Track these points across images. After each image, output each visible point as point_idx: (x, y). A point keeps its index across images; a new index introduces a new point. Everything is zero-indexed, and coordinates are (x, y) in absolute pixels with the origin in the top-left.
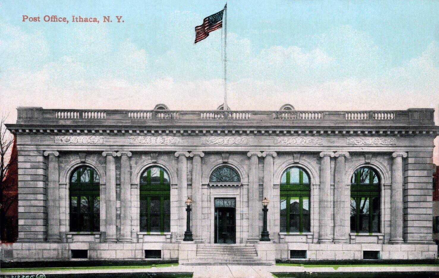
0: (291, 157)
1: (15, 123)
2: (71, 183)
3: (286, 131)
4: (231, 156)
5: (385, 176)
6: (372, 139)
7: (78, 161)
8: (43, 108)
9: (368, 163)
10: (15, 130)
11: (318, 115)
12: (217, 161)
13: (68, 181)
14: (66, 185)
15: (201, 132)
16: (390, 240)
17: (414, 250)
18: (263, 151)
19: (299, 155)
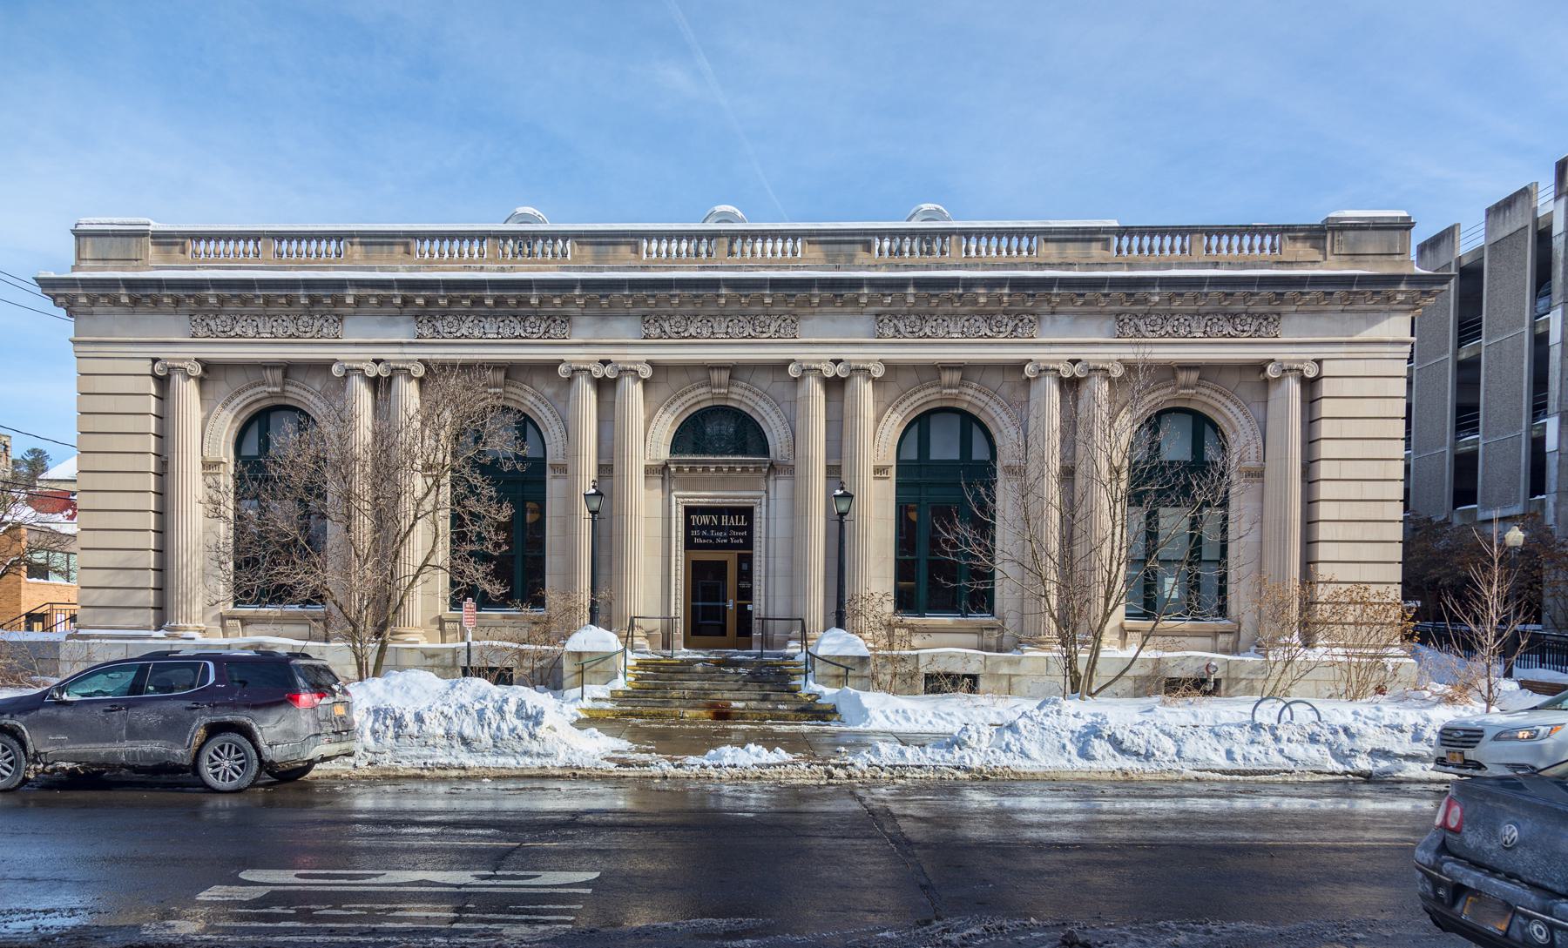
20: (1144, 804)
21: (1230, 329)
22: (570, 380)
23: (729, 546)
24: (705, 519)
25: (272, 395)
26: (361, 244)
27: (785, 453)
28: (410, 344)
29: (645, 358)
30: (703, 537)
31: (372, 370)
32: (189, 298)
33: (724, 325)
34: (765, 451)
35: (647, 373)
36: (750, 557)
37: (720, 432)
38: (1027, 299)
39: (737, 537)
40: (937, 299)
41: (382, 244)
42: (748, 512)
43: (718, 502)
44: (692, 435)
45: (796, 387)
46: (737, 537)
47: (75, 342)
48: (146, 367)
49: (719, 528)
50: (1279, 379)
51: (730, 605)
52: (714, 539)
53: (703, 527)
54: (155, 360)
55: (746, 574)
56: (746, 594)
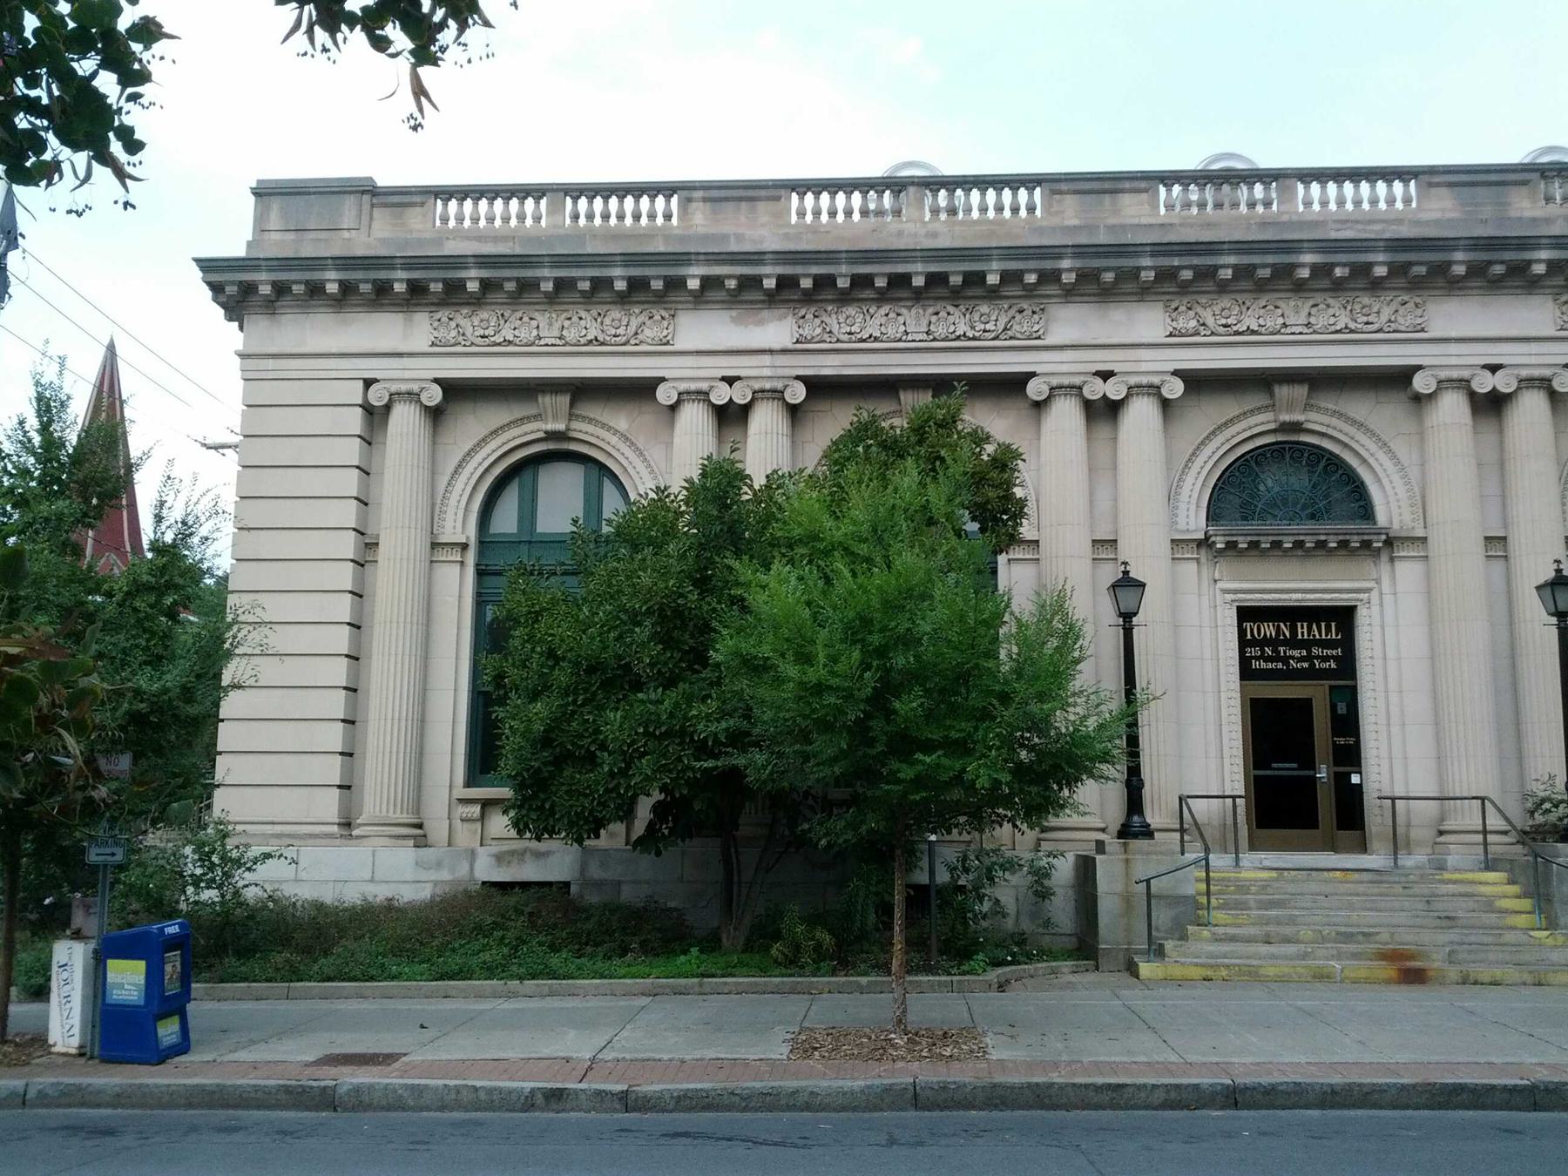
0: (1256, 400)
1: (240, 251)
2: (486, 542)
3: (623, 278)
4: (1328, 401)
5: (1390, 491)
6: (918, 319)
7: (1262, 421)
8: (379, 184)
9: (1296, 427)
10: (274, 284)
11: (1015, 195)
12: (1252, 424)
13: (472, 532)
14: (464, 547)
15: (756, 281)
16: (1441, 833)
17: (368, 876)
18: (738, 378)
19: (1301, 391)
20: (61, 1111)
21: (967, 329)
22: (673, 408)
23: (1312, 674)
24: (1268, 630)
25: (552, 436)
26: (705, 200)
27: (1407, 518)
28: (784, 351)
29: (1171, 367)
30: (1268, 659)
31: (721, 395)
32: (431, 286)
33: (557, 325)
34: (1366, 511)
35: (797, 393)
36: (1353, 691)
37: (1290, 490)
38: (650, 282)
39: (1325, 659)
40: (1272, 268)
41: (741, 199)
42: (1344, 617)
43: (1294, 599)
44: (1236, 491)
45: (671, 423)
46: (1325, 659)
47: (242, 356)
48: (355, 393)
49: (1294, 643)
50: (1431, 396)
51: (1322, 774)
52: (1285, 660)
53: (1266, 642)
54: (368, 383)
55: (1347, 723)
56: (1350, 756)
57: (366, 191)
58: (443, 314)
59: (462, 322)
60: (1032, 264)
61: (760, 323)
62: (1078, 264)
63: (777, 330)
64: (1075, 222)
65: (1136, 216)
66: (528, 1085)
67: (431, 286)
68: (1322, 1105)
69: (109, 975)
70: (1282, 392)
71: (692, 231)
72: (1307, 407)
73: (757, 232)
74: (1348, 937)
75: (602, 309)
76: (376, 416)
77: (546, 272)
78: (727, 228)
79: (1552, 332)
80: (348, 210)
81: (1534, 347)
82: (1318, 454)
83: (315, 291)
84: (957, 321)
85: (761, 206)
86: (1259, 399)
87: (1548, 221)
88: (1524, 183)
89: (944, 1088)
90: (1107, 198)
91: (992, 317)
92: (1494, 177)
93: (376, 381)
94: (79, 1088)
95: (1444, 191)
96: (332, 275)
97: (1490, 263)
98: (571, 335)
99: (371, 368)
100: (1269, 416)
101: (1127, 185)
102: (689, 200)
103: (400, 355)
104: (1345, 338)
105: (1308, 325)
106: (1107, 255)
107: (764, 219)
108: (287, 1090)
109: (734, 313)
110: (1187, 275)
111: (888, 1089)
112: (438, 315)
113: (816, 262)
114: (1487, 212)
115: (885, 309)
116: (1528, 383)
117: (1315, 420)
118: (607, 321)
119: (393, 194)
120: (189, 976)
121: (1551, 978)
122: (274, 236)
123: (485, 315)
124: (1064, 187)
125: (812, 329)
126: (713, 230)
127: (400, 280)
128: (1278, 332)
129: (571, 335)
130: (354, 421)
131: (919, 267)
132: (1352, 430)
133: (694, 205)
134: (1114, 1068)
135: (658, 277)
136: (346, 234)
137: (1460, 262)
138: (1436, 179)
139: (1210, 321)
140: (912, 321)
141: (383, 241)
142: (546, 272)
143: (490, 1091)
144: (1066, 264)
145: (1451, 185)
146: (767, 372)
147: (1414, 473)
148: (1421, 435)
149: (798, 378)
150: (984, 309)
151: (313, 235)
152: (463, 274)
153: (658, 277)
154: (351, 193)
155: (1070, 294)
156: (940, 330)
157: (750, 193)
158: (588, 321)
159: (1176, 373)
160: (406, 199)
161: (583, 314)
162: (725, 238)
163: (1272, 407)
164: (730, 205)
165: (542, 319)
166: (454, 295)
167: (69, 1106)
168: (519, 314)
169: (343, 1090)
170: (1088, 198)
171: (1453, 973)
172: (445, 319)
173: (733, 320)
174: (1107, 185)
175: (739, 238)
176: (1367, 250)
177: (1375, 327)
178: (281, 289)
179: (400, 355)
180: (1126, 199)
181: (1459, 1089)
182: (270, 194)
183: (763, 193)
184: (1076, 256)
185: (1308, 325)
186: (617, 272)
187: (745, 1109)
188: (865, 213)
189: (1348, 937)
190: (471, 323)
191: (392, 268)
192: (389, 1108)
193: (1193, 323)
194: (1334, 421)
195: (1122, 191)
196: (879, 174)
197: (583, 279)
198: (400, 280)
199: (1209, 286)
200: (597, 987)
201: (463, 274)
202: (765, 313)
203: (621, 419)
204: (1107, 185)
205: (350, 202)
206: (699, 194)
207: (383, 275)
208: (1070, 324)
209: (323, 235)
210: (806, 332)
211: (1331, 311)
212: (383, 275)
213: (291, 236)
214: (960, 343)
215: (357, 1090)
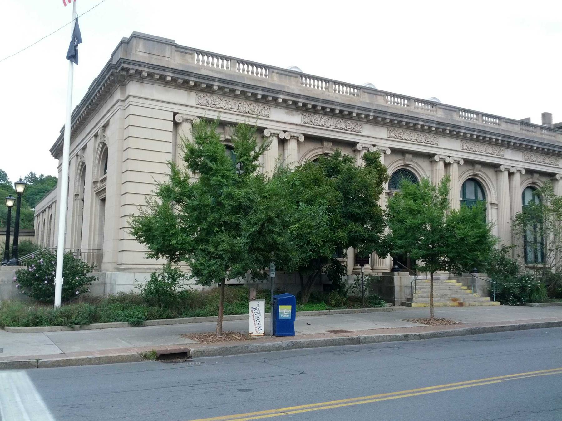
3: (261, 94)
4: (484, 170)
19: (410, 156)
26: (277, 73)
28: (300, 125)
32: (201, 85)
35: (302, 139)
54: (175, 114)
57: (171, 44)
58: (202, 94)
59: (207, 98)
60: (364, 112)
61: (293, 115)
62: (374, 114)
63: (297, 118)
64: (368, 101)
65: (457, 119)
66: (401, 334)
67: (201, 85)
68: (511, 330)
69: (290, 311)
70: (326, 144)
71: (274, 82)
72: (411, 161)
73: (293, 86)
74: (442, 296)
75: (250, 102)
76: (176, 125)
77: (239, 88)
78: (283, 84)
79: (460, 150)
80: (168, 51)
81: (457, 153)
82: (410, 172)
83: (162, 79)
84: (342, 124)
85: (292, 78)
86: (319, 145)
87: (460, 122)
88: (455, 111)
89: (476, 329)
90: (375, 96)
91: (351, 125)
92: (450, 109)
93: (178, 113)
94: (298, 343)
95: (441, 110)
96: (170, 74)
97: (453, 131)
98: (241, 109)
99: (177, 109)
100: (321, 150)
101: (379, 94)
102: (273, 72)
103: (187, 106)
104: (423, 144)
105: (416, 140)
106: (413, 119)
107: (294, 83)
108: (349, 339)
109: (286, 111)
110: (227, 90)
111: (467, 330)
112: (200, 94)
113: (314, 101)
114: (449, 117)
115: (326, 117)
116: (293, 137)
117: (412, 164)
118: (252, 106)
119: (181, 48)
120: (295, 309)
121: (483, 304)
122: (140, 53)
123: (215, 97)
124: (366, 91)
125: (307, 120)
126: (280, 83)
127: (193, 81)
128: (229, 110)
129: (419, 139)
130: (170, 125)
131: (338, 108)
132: (419, 168)
133: (274, 74)
134: (502, 323)
135: (270, 96)
136: (167, 59)
137: (216, 85)
138: (440, 107)
139: (397, 135)
140: (331, 122)
141: (180, 64)
142: (388, 117)
143: (393, 336)
144: (371, 114)
145: (442, 109)
146: (295, 131)
147: (496, 187)
148: (497, 179)
149: (303, 134)
150: (349, 122)
151: (155, 56)
152: (213, 83)
153: (270, 96)
154: (169, 44)
155: (368, 122)
156: (339, 126)
157: (290, 74)
158: (342, 123)
159: (390, 148)
160: (187, 51)
161: (245, 103)
162: (284, 87)
163: (473, 169)
164: (284, 76)
165: (232, 102)
166: (209, 90)
167: (296, 348)
168: (226, 99)
169: (362, 338)
170: (448, 111)
171: (468, 304)
172: (202, 96)
173: (287, 113)
174: (375, 93)
175: (288, 88)
176: (402, 117)
177: (256, 113)
178: (150, 75)
179: (187, 106)
180: (379, 97)
181: (549, 324)
182: (140, 38)
183: (293, 75)
184: (374, 112)
185: (416, 140)
186: (145, 69)
187: (442, 337)
188: (350, 93)
189: (442, 296)
190: (213, 100)
191: (191, 76)
192: (372, 342)
193: (394, 135)
194: (415, 165)
195: (378, 95)
196: (426, 99)
197: (249, 92)
198: (193, 81)
199: (232, 95)
200: (158, 322)
201: (213, 83)
202: (294, 113)
203: (490, 173)
204: (375, 93)
205: (168, 48)
206: (276, 71)
207: (187, 78)
208: (367, 130)
209: (159, 57)
210: (201, 101)
211: (245, 106)
212: (187, 78)
213: (147, 55)
214: (343, 131)
215: (365, 338)
